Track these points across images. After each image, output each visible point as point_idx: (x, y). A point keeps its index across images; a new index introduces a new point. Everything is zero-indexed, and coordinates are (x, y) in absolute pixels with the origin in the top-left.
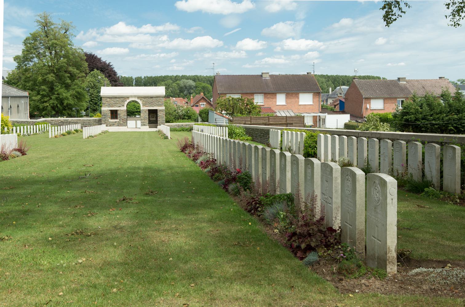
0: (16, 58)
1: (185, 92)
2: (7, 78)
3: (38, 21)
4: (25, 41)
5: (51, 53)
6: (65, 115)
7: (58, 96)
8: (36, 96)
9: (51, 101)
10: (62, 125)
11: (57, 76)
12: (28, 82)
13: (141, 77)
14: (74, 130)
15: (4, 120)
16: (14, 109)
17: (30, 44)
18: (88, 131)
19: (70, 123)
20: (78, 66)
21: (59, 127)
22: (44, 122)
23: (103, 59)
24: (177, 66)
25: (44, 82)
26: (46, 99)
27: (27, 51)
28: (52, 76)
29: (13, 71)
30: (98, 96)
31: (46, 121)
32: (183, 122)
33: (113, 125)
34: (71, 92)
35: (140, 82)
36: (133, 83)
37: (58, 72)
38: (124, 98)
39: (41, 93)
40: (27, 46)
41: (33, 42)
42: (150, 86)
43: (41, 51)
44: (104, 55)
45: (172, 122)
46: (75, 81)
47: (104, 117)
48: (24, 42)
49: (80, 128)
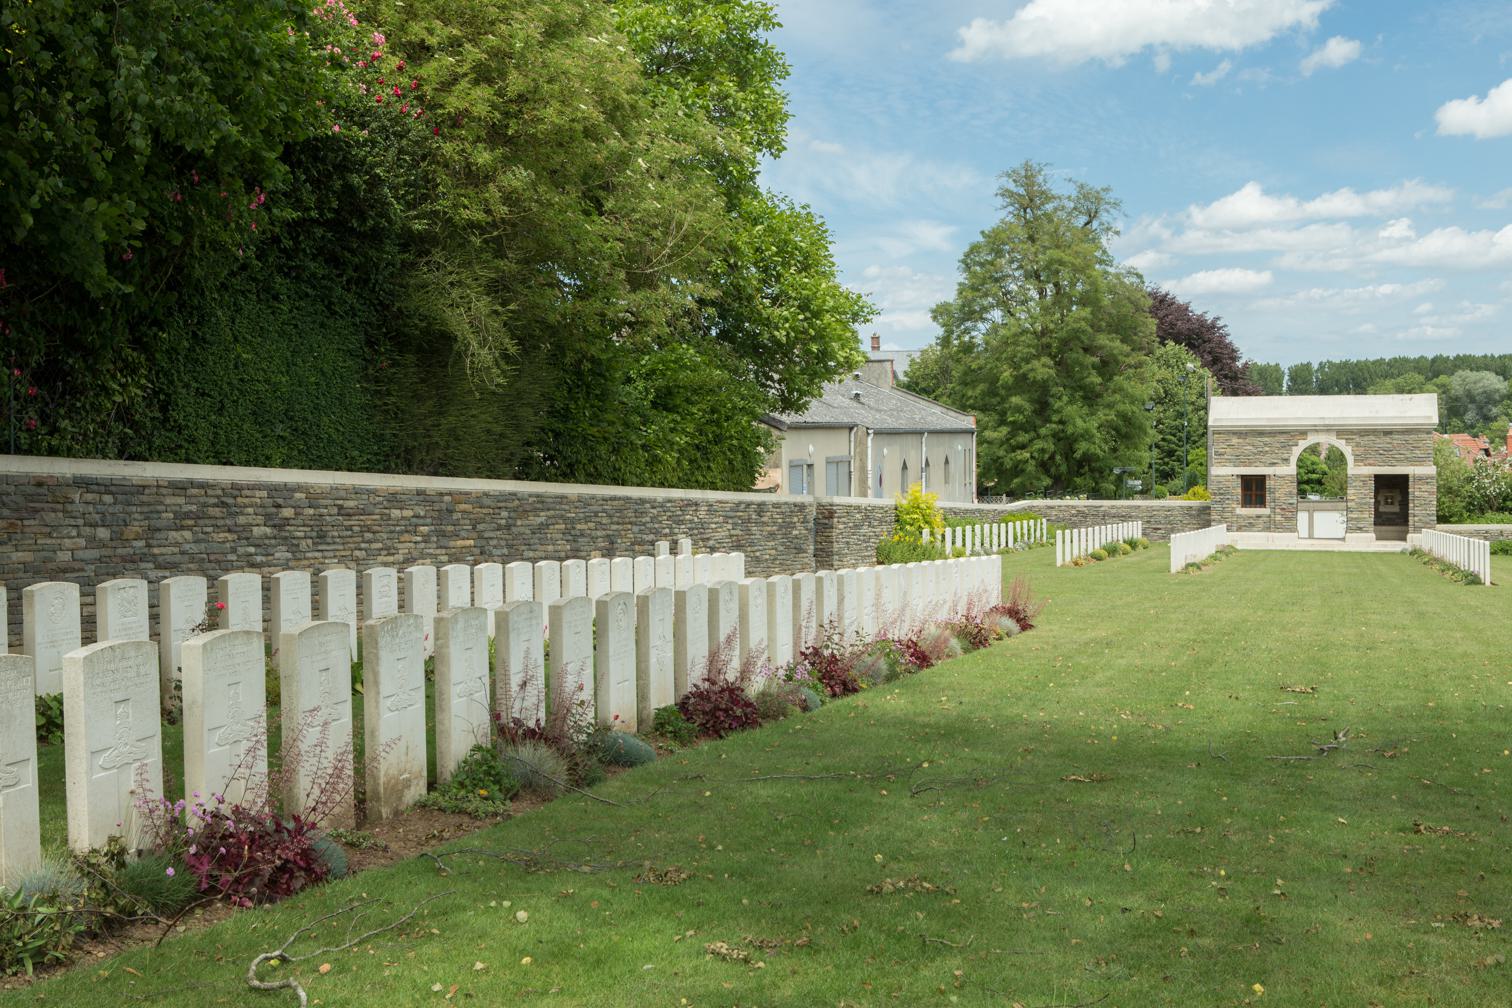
0: (939, 312)
1: (1470, 416)
2: (906, 374)
3: (1006, 193)
4: (967, 255)
5: (1042, 292)
6: (1083, 492)
7: (1061, 427)
8: (995, 429)
9: (1039, 445)
10: (1074, 525)
11: (1058, 364)
12: (973, 384)
13: (1309, 364)
14: (1125, 542)
15: (922, 506)
16: (937, 471)
17: (982, 265)
18: (1189, 546)
19: (1104, 518)
20: (1123, 329)
21: (968, 528)
22: (1026, 514)
23: (1197, 309)
24: (1433, 326)
25: (1022, 383)
26: (1023, 438)
27: (974, 288)
28: (1044, 365)
29: (923, 352)
30: (1177, 428)
31: (1031, 508)
32: (1502, 521)
33: (1248, 525)
34: (1103, 415)
35: (1304, 382)
36: (1281, 385)
37: (1061, 348)
38: (1287, 435)
39: (1011, 419)
40: (974, 275)
41: (989, 258)
42: (1340, 392)
43: (1013, 287)
44: (1196, 291)
45: (1460, 522)
46: (1116, 378)
47: (1218, 498)
48: (963, 261)
49: (1140, 536)
